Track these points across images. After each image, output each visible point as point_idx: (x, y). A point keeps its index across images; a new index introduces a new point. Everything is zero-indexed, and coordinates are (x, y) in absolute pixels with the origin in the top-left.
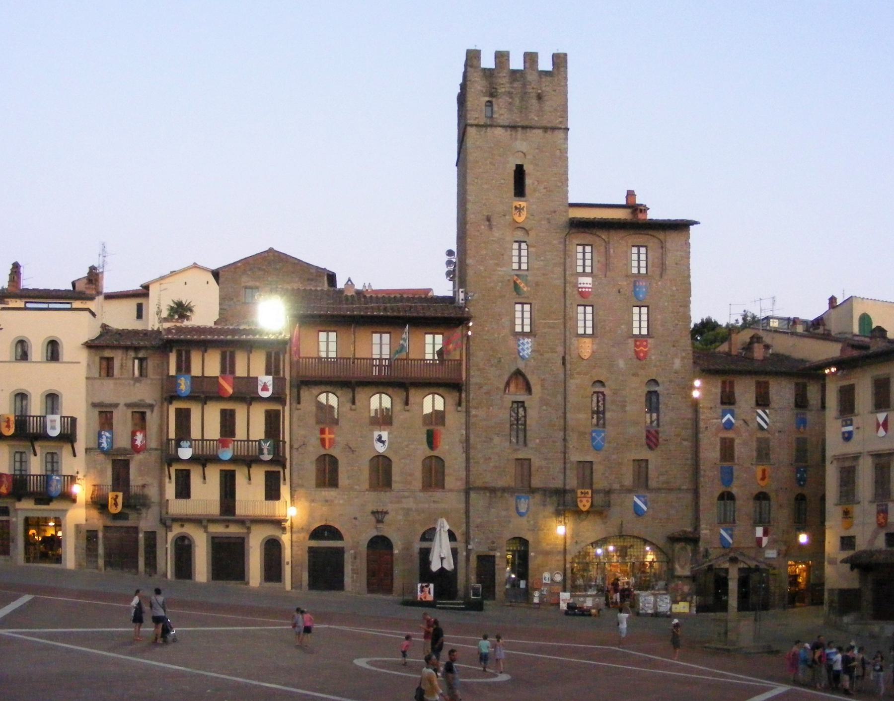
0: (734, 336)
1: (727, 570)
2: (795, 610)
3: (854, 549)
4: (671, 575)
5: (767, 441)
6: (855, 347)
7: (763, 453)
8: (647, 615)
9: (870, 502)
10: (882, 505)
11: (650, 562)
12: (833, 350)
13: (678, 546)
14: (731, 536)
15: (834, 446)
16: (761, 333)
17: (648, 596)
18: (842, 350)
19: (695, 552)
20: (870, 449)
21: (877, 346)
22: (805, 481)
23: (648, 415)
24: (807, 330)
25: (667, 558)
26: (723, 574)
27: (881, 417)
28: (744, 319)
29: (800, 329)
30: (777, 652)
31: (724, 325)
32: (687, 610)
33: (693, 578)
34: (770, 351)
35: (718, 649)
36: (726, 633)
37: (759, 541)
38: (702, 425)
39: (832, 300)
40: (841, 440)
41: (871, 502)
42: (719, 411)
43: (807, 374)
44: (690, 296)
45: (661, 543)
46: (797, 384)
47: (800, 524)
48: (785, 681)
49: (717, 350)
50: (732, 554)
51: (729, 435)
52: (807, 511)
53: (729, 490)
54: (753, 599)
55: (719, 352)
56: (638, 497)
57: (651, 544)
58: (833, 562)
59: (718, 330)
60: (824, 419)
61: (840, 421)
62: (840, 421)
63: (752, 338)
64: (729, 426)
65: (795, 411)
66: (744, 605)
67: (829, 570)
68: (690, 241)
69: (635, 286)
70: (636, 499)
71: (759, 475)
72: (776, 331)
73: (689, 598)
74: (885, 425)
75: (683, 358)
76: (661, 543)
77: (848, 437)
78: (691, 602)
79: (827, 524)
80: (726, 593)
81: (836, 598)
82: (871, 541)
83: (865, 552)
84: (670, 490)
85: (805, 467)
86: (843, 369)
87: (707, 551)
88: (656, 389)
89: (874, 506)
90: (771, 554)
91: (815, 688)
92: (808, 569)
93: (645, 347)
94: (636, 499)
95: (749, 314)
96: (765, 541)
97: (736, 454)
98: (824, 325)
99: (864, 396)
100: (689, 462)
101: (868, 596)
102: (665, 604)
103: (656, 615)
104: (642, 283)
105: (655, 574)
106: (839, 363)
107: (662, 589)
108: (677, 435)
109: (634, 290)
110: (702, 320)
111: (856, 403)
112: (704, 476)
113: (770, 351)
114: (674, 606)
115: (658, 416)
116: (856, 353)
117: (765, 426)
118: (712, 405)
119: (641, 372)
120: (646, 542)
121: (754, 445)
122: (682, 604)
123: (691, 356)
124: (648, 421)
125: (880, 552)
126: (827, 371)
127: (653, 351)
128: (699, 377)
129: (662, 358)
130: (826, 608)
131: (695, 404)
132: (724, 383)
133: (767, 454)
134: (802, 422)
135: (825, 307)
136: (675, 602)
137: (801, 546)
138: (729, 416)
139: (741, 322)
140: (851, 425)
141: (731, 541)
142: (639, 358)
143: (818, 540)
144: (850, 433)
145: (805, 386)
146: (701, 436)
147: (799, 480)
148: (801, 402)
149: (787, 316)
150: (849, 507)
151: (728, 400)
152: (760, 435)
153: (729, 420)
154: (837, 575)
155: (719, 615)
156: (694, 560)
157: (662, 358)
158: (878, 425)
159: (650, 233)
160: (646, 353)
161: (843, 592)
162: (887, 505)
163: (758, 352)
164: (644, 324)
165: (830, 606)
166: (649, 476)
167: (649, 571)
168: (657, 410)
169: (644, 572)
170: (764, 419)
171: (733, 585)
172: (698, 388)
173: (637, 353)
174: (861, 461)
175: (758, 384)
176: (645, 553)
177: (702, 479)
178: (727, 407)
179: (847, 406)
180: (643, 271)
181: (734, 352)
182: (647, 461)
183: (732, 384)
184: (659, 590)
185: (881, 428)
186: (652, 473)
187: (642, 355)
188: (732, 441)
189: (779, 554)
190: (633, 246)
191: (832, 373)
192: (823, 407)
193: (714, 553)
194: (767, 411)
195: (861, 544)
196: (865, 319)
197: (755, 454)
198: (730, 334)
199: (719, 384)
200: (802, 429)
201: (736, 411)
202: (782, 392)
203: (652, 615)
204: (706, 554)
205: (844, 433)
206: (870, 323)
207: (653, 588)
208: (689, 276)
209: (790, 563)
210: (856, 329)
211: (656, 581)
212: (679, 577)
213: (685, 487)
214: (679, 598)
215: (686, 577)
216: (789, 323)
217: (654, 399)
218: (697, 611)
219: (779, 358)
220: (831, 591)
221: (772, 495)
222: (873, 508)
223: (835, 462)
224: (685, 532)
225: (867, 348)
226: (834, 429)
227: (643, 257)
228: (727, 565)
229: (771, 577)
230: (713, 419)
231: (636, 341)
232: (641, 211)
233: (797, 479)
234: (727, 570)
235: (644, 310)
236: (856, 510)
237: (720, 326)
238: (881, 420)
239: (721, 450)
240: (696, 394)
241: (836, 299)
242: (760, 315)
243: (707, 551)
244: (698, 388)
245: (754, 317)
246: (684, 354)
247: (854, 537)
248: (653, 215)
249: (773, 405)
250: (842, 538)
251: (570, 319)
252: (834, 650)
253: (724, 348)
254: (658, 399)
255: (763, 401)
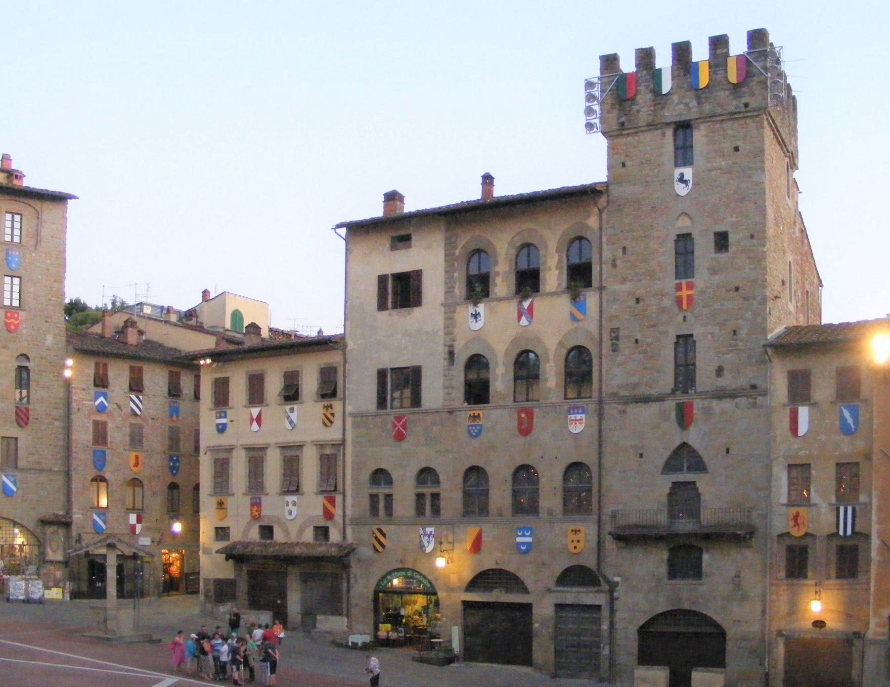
0: (107, 319)
1: (104, 556)
2: (171, 598)
3: (228, 540)
4: (43, 560)
5: (141, 427)
6: (231, 341)
7: (136, 439)
8: (17, 601)
9: (210, 495)
10: (256, 498)
11: (20, 546)
12: (209, 343)
13: (50, 530)
14: (104, 522)
15: (208, 437)
16: (135, 318)
17: (19, 580)
18: (217, 344)
19: (68, 537)
20: (244, 443)
21: (250, 342)
22: (177, 470)
23: (18, 391)
24: (180, 320)
25: (40, 544)
26: (99, 560)
27: (255, 411)
28: (113, 303)
29: (173, 318)
30: (159, 641)
31: (94, 307)
32: (60, 597)
33: (66, 563)
34: (144, 337)
35: (99, 638)
36: (105, 621)
37: (133, 528)
38: (74, 405)
39: (205, 293)
40: (215, 432)
41: (245, 494)
42: (92, 393)
43: (183, 363)
44: (65, 272)
45: (31, 525)
46: (171, 372)
47: (174, 512)
48: (171, 672)
49: (90, 330)
50: (109, 541)
51: (101, 418)
52: (181, 498)
53: (102, 474)
54: (128, 586)
55: (92, 333)
56: (7, 476)
57: (22, 526)
58: (207, 552)
59: (87, 312)
60: (198, 410)
61: (214, 412)
62: (214, 412)
63: (126, 322)
64: (101, 409)
65: (170, 399)
66: (121, 594)
67: (204, 559)
68: (68, 215)
69: (7, 255)
70: (5, 479)
71: (133, 462)
72: (149, 318)
73: (61, 584)
74: (259, 420)
75: (55, 335)
76: (31, 525)
77: (221, 429)
78: (64, 588)
79: (201, 513)
80: (103, 579)
81: (211, 587)
82: (245, 534)
83: (239, 543)
84: (41, 471)
85: (178, 456)
86: (218, 362)
87: (80, 536)
88: (27, 364)
89: (248, 498)
90: (145, 541)
91: (202, 679)
92: (182, 558)
93: (17, 319)
94: (5, 479)
95: (118, 300)
96: (139, 528)
97: (109, 439)
98: (197, 317)
99: (238, 389)
100: (61, 443)
101: (243, 588)
102: (37, 590)
103: (28, 601)
104: (15, 253)
105: (25, 557)
106: (218, 356)
107: (33, 574)
108: (48, 415)
109: (7, 259)
110: (71, 300)
111: (230, 394)
112: (76, 458)
113: (144, 337)
114: (46, 592)
115: (28, 393)
116: (232, 347)
117: (139, 413)
118: (84, 386)
119: (11, 345)
120: (15, 524)
121: (127, 430)
122: (54, 590)
123: (64, 333)
124: (18, 396)
125: (253, 544)
126: (202, 362)
127: (24, 325)
128: (72, 357)
129: (34, 333)
130: (202, 597)
131: (67, 384)
132: (97, 364)
133: (140, 441)
134: (174, 411)
135: (200, 300)
136: (47, 587)
137: (174, 535)
138: (102, 399)
139: (110, 307)
140: (225, 417)
141: (104, 527)
142: (9, 331)
143: (193, 531)
144: (224, 425)
145: (178, 375)
146: (73, 417)
147: (172, 469)
148: (174, 392)
149: (160, 304)
150: (223, 499)
151: (101, 382)
152: (133, 420)
153: (102, 402)
154: (212, 566)
155: (95, 602)
156: (67, 545)
157: (34, 333)
158: (252, 420)
159: (26, 201)
160: (17, 326)
161: (219, 583)
162: (260, 499)
163: (132, 338)
164: (16, 296)
165: (206, 595)
166: (19, 455)
167: (18, 554)
168: (28, 387)
169: (13, 556)
170: (135, 406)
171: (111, 573)
172: (71, 368)
173: (7, 325)
174: (234, 453)
175: (132, 369)
176: (14, 536)
177: (74, 462)
178: (101, 390)
179: (221, 399)
180: (17, 239)
181: (107, 335)
182: (16, 439)
183: (105, 366)
184: (29, 575)
185: (255, 423)
186: (21, 453)
187: (12, 327)
188: (105, 424)
189: (153, 542)
190: (7, 212)
191: (206, 364)
192: (197, 397)
193: (87, 539)
194: (141, 397)
195: (236, 536)
196: (237, 316)
197: (128, 439)
198: (103, 316)
199: (93, 365)
200: (174, 418)
201: (109, 394)
202: (156, 379)
203: (23, 601)
204: (79, 539)
205: (218, 425)
206: (241, 320)
207: (24, 573)
208: (64, 251)
209: (163, 551)
210: (228, 325)
211: (27, 565)
212: (52, 562)
213: (56, 469)
214: (51, 584)
215: (59, 562)
216: (162, 311)
217: (24, 375)
218: (71, 599)
219: (150, 345)
220: (207, 581)
221: (145, 482)
222: (247, 500)
223: (209, 453)
224: (56, 515)
225: (240, 343)
226: (208, 420)
227: (17, 225)
228: (103, 551)
229: (146, 565)
230: (85, 399)
231: (6, 312)
232: (16, 176)
233: (170, 467)
234: (104, 556)
235: (16, 281)
236: (230, 502)
237: (91, 308)
238: (255, 416)
239: (94, 432)
240: (68, 373)
241: (209, 292)
242: (131, 302)
243: (80, 536)
244: (71, 368)
245: (123, 303)
246: (57, 331)
247: (228, 528)
248: (30, 182)
249: (146, 391)
250: (217, 528)
251: (410, 221)
252: (220, 641)
253: (97, 329)
254: (28, 377)
255: (136, 386)
